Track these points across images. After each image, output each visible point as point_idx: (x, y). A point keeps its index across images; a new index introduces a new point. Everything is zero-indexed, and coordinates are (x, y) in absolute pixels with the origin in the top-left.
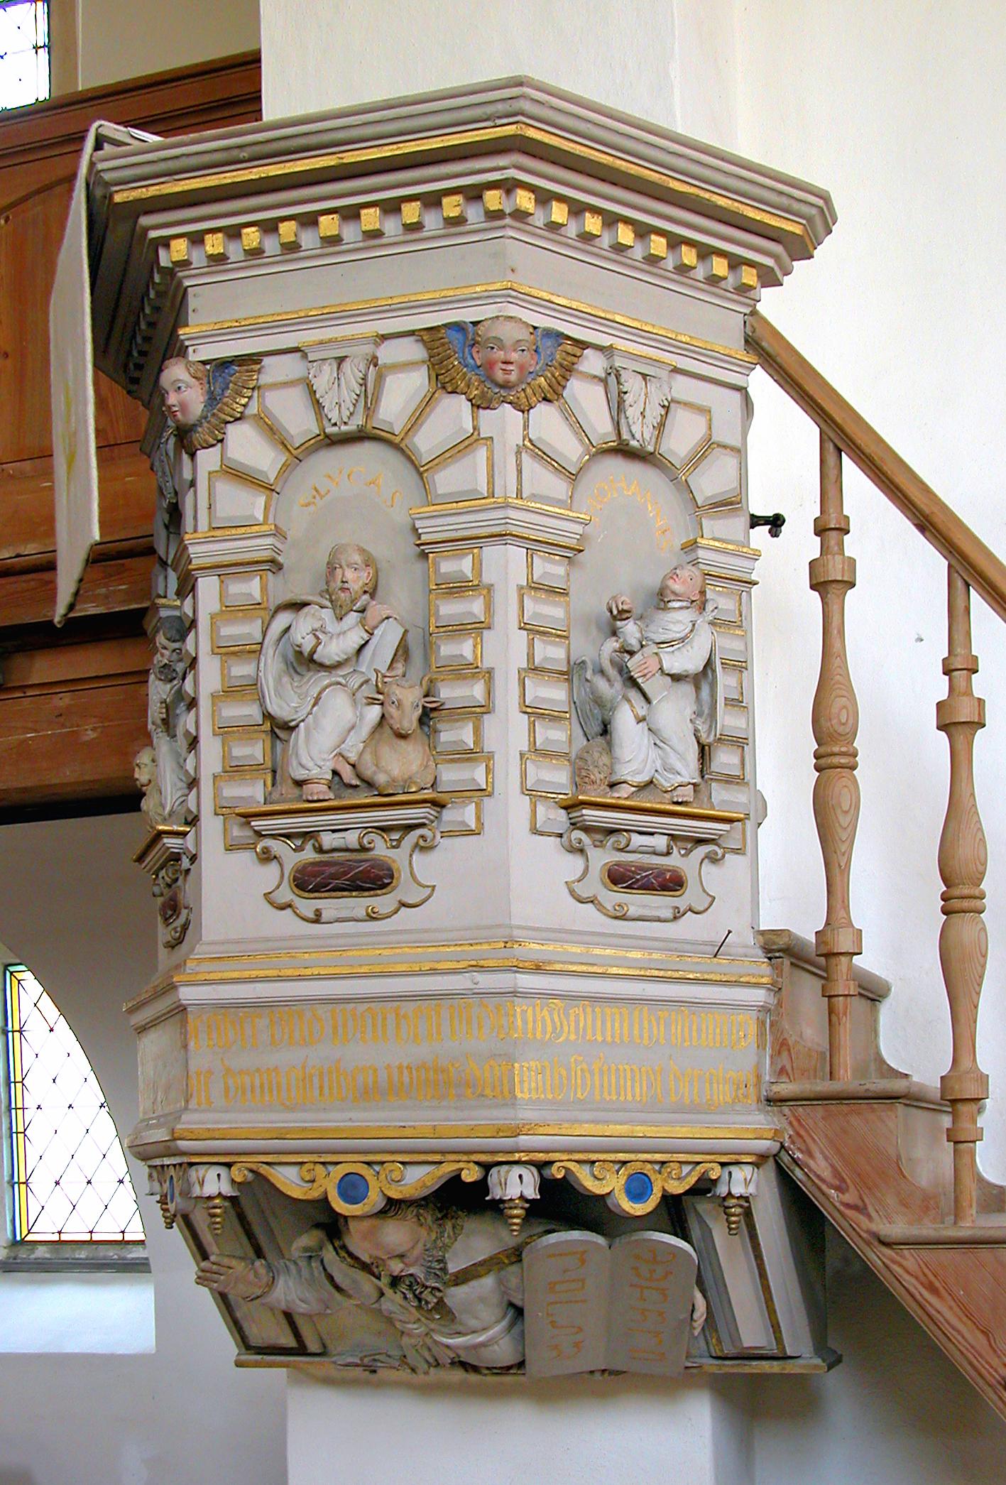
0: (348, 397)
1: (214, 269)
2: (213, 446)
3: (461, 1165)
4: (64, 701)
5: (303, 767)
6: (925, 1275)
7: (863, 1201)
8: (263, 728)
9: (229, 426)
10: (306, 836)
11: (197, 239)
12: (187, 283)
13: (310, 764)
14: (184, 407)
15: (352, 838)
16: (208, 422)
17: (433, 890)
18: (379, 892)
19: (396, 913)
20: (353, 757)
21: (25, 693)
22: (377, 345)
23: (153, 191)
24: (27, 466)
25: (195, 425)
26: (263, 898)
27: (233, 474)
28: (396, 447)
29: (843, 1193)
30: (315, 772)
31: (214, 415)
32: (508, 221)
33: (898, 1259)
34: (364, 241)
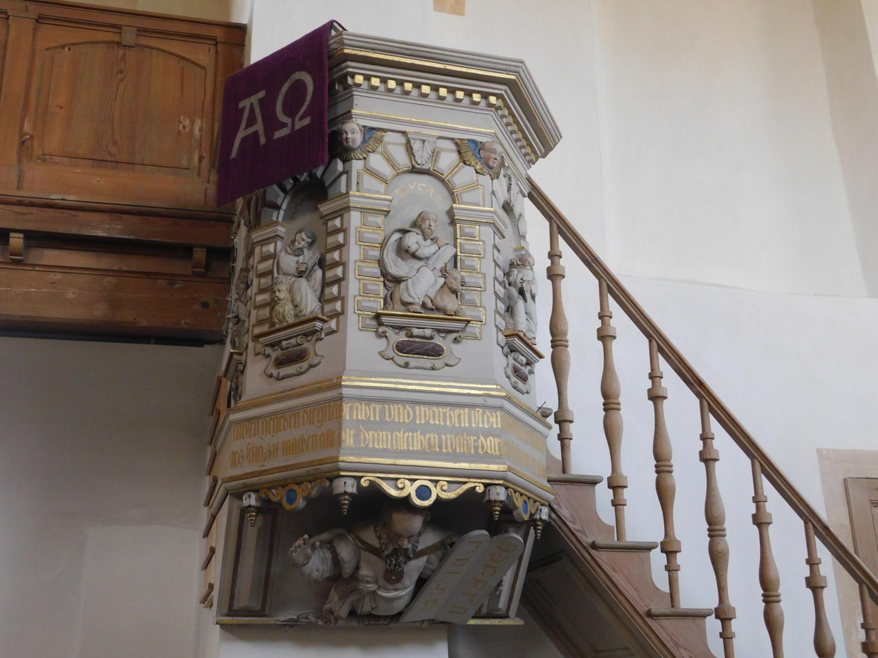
0: (426, 156)
1: (369, 91)
2: (360, 159)
3: (476, 484)
4: (57, 277)
5: (411, 296)
6: (611, 564)
7: (583, 528)
8: (380, 280)
9: (370, 153)
10: (401, 328)
11: (367, 78)
12: (354, 93)
13: (415, 297)
14: (354, 141)
15: (428, 332)
16: (361, 150)
17: (460, 361)
18: (436, 358)
19: (443, 368)
20: (432, 296)
21: (34, 268)
22: (437, 139)
23: (362, 53)
24: (66, 160)
25: (355, 149)
26: (378, 353)
27: (368, 173)
28: (442, 181)
29: (575, 525)
30: (417, 300)
31: (364, 147)
32: (493, 109)
33: (600, 556)
34: (436, 99)
